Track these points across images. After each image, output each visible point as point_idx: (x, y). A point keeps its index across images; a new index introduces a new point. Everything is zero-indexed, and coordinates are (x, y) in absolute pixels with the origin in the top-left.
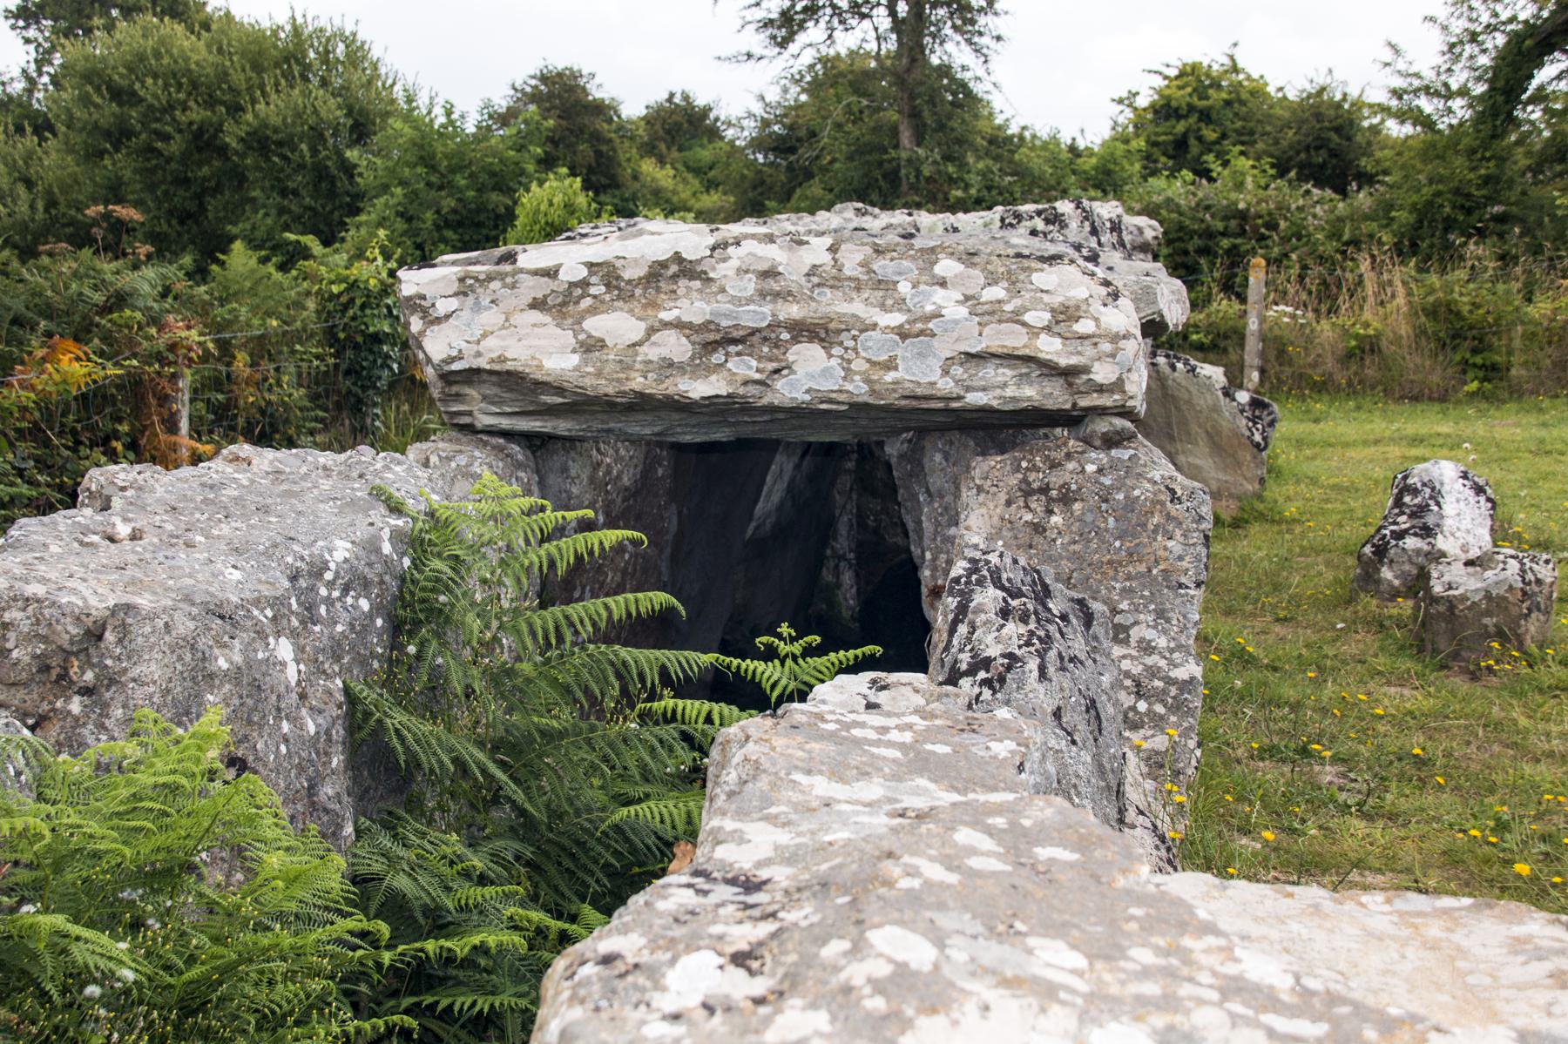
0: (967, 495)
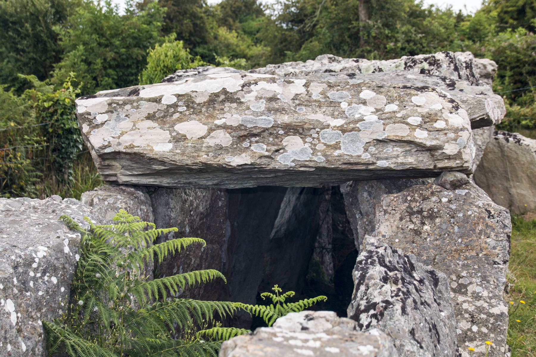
0: (379, 215)
